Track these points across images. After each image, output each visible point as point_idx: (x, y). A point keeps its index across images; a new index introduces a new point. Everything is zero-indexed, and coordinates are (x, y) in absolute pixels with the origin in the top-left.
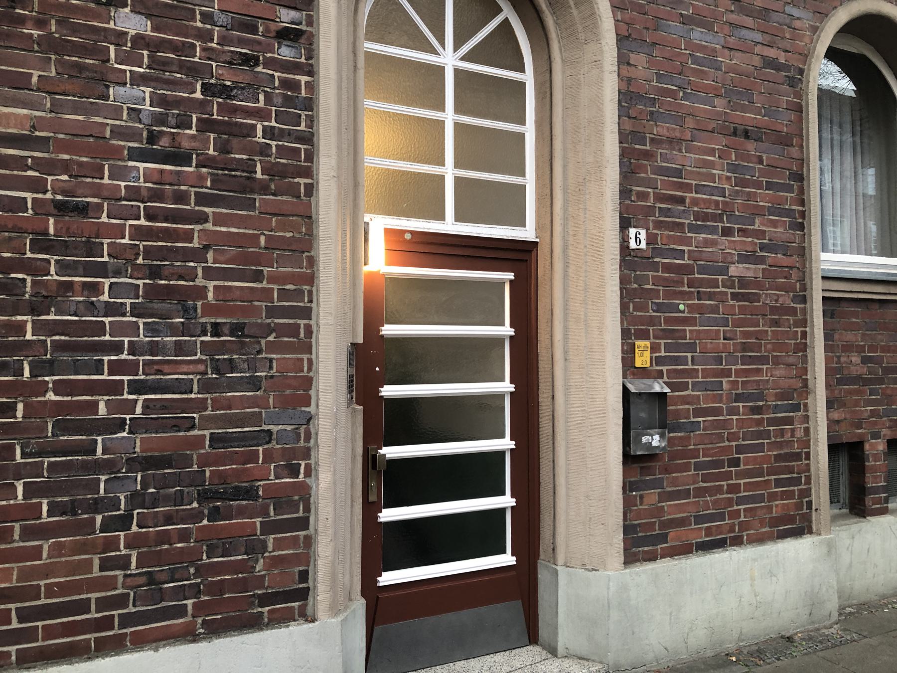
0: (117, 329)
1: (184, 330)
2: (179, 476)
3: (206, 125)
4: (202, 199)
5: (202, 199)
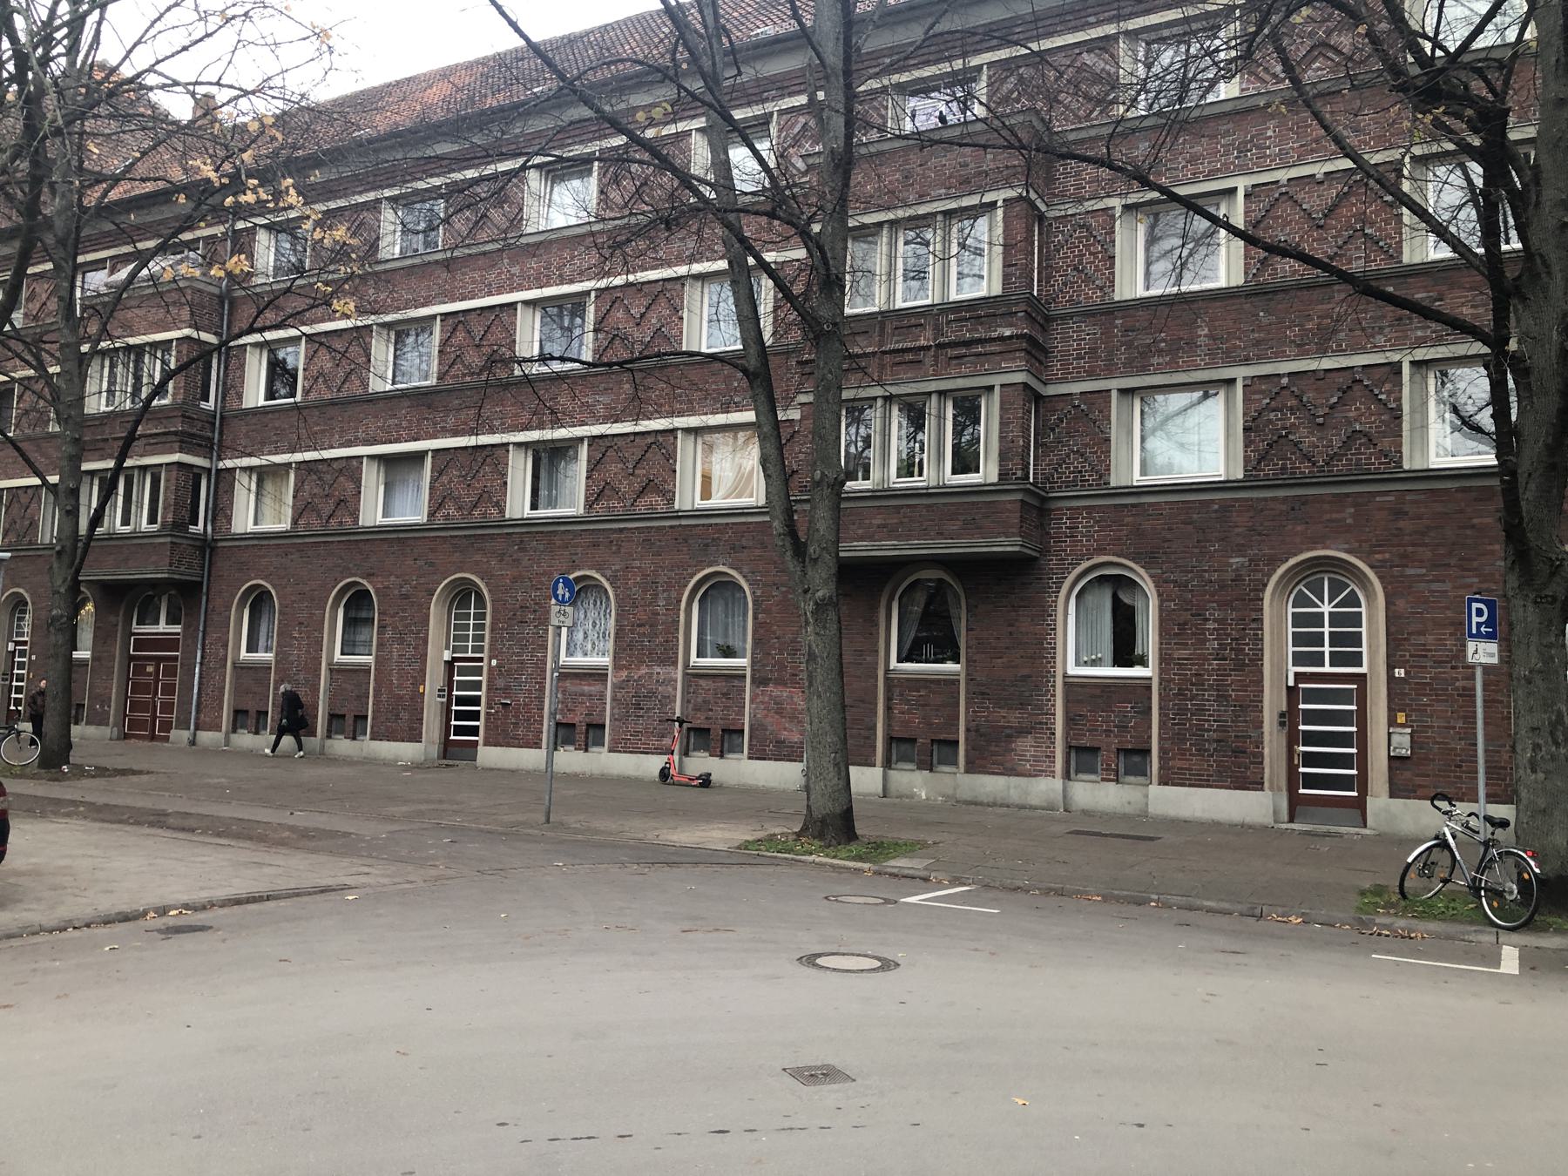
0: (1210, 706)
1: (1226, 706)
2: (916, 326)
3: (1231, 649)
4: (1231, 670)
5: (1231, 670)
